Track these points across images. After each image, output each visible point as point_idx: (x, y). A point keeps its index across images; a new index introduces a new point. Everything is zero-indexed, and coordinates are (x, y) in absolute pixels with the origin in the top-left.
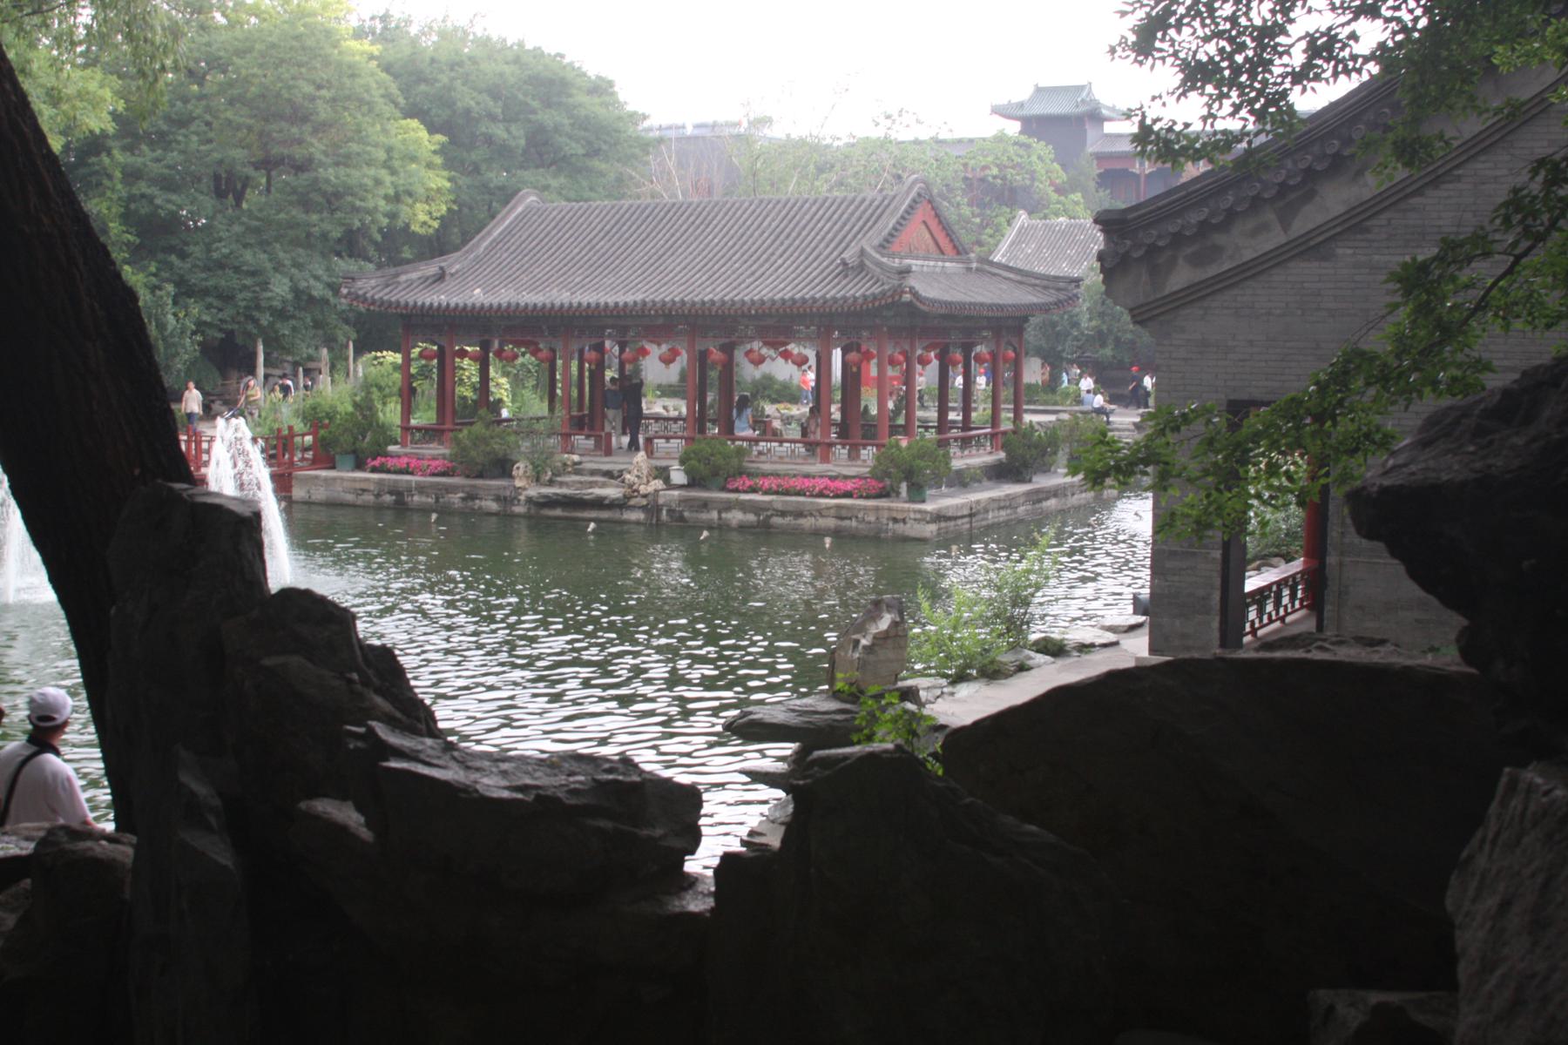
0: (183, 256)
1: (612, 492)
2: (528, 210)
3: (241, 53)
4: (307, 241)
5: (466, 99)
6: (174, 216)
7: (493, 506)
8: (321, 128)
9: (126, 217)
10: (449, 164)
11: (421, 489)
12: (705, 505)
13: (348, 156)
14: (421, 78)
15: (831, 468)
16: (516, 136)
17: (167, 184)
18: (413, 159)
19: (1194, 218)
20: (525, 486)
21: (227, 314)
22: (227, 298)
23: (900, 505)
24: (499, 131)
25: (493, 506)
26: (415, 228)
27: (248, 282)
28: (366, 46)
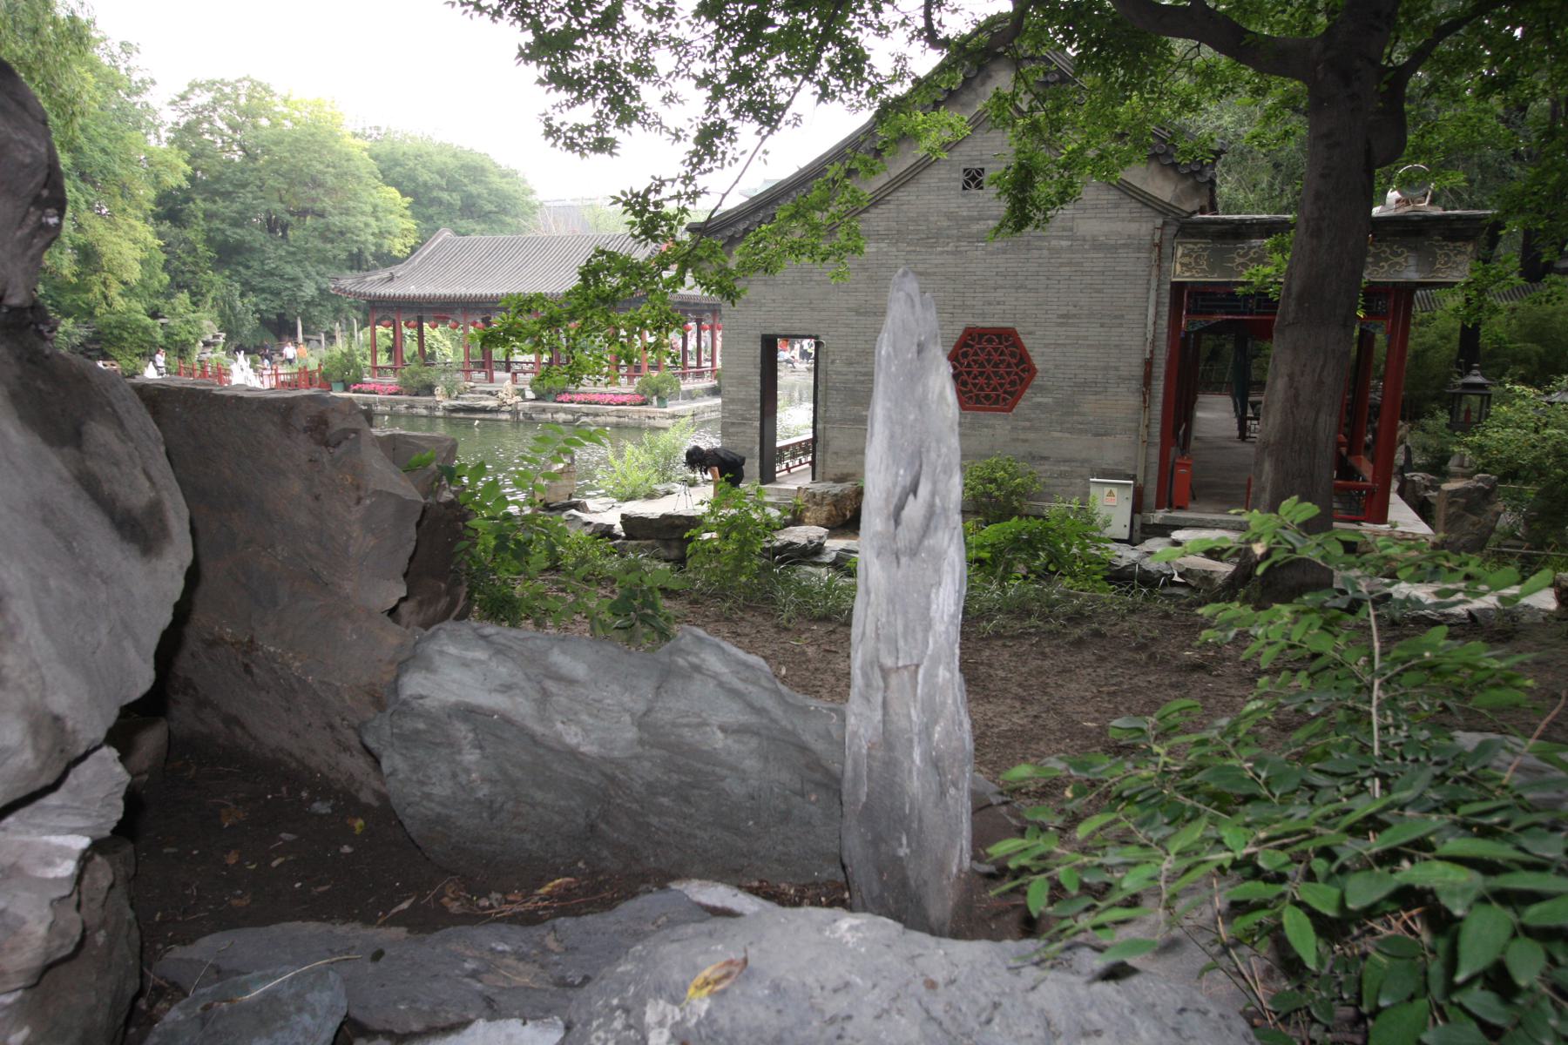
0: (248, 267)
1: (491, 403)
2: (445, 240)
3: (277, 143)
4: (324, 261)
5: (424, 176)
6: (243, 242)
7: (424, 412)
8: (330, 191)
9: (209, 241)
10: (415, 216)
11: (382, 402)
12: (544, 410)
13: (347, 209)
14: (397, 163)
15: (616, 389)
16: (455, 199)
17: (236, 223)
18: (391, 212)
19: (741, 227)
20: (442, 399)
21: (277, 303)
22: (277, 294)
23: (651, 409)
24: (445, 196)
25: (424, 412)
26: (395, 253)
27: (289, 285)
28: (359, 142)
